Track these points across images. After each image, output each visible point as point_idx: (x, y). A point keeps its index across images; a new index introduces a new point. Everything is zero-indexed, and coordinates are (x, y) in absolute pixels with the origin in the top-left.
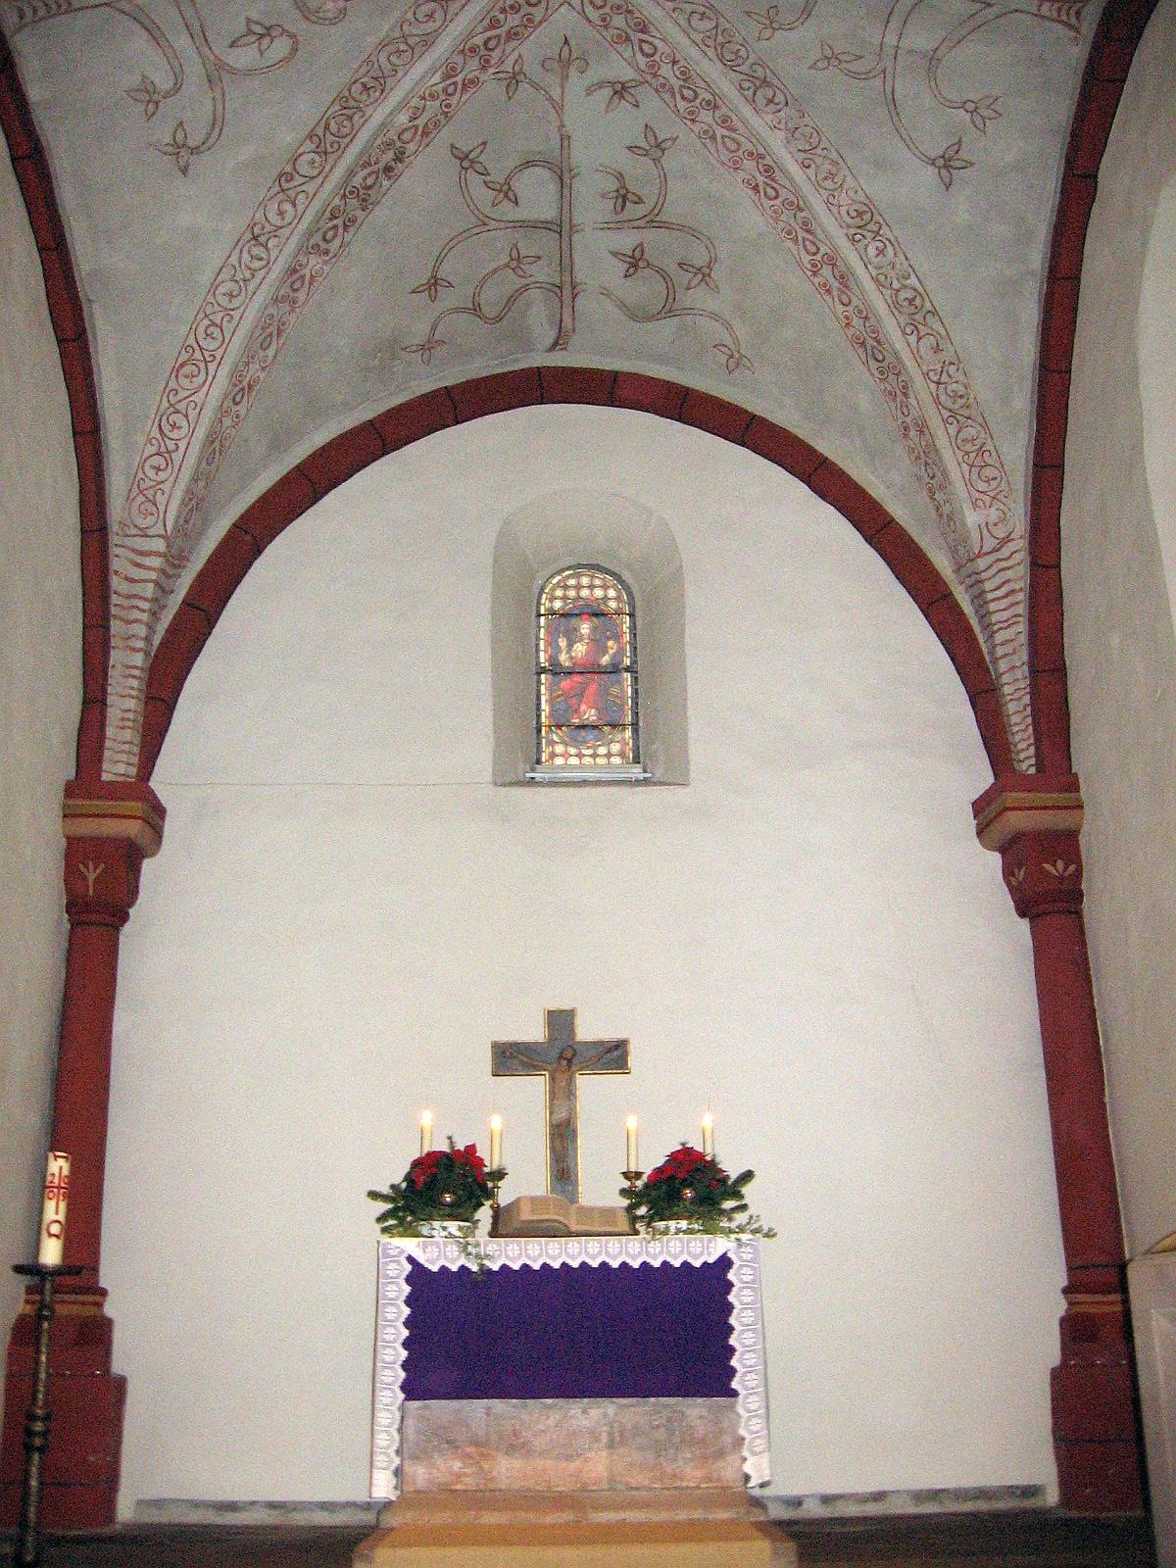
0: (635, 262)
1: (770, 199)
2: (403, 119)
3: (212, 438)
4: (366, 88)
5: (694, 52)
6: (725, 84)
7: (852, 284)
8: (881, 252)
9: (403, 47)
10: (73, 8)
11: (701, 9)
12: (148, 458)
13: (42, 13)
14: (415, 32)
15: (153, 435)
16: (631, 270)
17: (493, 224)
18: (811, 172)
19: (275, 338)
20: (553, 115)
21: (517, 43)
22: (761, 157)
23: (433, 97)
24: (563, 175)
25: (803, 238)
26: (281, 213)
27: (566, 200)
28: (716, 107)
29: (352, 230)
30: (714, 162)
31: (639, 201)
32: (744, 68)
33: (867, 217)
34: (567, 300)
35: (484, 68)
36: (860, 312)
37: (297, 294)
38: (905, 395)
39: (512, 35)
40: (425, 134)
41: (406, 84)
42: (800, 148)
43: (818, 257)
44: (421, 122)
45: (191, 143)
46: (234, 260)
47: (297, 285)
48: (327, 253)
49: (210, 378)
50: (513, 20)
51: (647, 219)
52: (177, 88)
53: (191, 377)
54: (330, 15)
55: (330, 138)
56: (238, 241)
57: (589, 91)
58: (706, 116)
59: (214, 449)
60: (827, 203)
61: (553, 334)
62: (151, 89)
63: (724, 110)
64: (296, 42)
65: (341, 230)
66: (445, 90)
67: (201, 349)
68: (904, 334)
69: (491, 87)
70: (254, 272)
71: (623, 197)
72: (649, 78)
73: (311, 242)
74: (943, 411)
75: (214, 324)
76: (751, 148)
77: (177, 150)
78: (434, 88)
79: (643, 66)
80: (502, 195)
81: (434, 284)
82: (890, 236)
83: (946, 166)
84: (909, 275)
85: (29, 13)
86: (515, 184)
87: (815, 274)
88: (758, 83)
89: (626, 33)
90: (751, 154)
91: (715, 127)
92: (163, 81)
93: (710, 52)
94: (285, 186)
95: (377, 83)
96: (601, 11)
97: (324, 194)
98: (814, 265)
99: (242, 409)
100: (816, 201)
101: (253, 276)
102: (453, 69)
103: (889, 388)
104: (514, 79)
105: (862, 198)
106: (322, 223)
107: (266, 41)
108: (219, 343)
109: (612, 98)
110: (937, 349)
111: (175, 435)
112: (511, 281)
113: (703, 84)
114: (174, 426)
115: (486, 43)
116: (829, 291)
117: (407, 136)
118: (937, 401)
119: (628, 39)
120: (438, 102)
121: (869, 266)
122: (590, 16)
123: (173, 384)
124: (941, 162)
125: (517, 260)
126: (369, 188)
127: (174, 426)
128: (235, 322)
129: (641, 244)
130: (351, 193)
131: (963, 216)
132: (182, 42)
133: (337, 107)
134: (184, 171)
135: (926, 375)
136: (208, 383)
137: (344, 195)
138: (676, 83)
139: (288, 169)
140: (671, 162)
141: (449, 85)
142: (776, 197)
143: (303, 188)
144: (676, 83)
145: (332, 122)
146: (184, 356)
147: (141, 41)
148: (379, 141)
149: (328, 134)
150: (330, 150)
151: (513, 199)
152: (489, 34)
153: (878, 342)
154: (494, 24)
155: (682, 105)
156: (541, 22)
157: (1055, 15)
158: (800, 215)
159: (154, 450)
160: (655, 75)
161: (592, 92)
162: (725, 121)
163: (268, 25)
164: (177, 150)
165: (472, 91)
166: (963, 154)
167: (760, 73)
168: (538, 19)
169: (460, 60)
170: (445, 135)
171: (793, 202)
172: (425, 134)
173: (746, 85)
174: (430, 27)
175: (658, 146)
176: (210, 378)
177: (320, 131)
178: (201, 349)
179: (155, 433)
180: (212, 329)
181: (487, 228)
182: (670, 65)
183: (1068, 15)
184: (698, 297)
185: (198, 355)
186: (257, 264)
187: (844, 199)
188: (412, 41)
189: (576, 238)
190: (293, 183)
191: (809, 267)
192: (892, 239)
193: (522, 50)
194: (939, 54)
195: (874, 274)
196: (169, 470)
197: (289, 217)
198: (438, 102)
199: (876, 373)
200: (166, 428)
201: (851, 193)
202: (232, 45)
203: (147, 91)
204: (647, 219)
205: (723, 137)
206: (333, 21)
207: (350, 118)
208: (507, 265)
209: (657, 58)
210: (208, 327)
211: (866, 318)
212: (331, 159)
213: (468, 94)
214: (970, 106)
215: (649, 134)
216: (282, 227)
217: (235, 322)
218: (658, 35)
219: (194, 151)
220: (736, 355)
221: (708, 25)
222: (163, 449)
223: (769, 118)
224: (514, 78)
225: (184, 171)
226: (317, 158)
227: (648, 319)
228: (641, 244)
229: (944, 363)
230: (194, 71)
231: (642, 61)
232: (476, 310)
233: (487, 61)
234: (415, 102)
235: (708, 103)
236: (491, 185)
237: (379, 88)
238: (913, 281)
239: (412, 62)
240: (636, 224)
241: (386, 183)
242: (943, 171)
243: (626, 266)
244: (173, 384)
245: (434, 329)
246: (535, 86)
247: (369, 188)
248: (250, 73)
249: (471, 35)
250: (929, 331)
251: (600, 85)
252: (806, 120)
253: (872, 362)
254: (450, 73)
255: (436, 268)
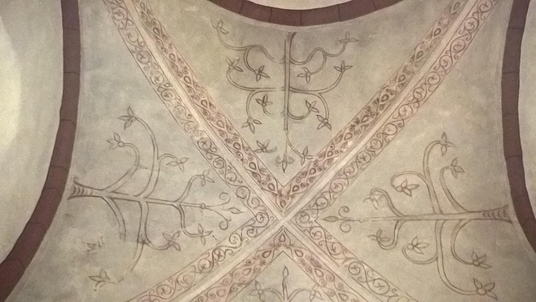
0: (260, 73)
1: (205, 100)
2: (350, 143)
3: (455, 15)
4: (364, 159)
5: (234, 164)
6: (223, 151)
7: (169, 64)
8: (157, 79)
9: (348, 174)
10: (482, 213)
11: (231, 183)
12: (488, 11)
13: (496, 213)
14: (343, 180)
15: (483, 21)
16: (261, 69)
17: (316, 93)
18: (188, 113)
19: (416, 54)
20: (290, 139)
21: (303, 171)
22: (208, 119)
23: (337, 152)
24: (287, 113)
25: (191, 83)
26: (405, 111)
27: (286, 102)
28: (226, 140)
29: (375, 98)
30: (227, 116)
31: (257, 100)
32: (215, 157)
33: (164, 94)
34: (288, 56)
35: (317, 161)
36: (165, 51)
37: (402, 74)
38: (142, 13)
39: (305, 174)
40: (341, 136)
41: (348, 158)
42: (192, 123)
43: (184, 75)
44: (343, 141)
45: (440, 146)
46: (429, 93)
47: (402, 78)
48: (387, 90)
49: (450, 44)
50: (304, 180)
51: (255, 92)
52: (443, 171)
53: (458, 45)
54: (377, 193)
55: (381, 139)
56: (425, 101)
57: (276, 149)
58: (231, 136)
59: (454, 9)
60: (180, 100)
61: (294, 40)
62: (454, 172)
63: (223, 139)
64: (391, 183)
65: (380, 100)
66: (332, 154)
67: (451, 57)
68: (145, 42)
69: (314, 153)
70: (421, 87)
71: (264, 102)
72: (252, 153)
73: (394, 96)
74: (124, 6)
75: (443, 67)
76: (212, 123)
77: (446, 144)
78: (337, 155)
79: (255, 158)
80: (312, 106)
81: (342, 69)
82: (154, 86)
83: (131, 117)
84: (144, 69)
85: (501, 213)
86: (307, 111)
87: (186, 68)
88: (209, 151)
89: (261, 173)
90: (212, 120)
91: (227, 132)
92: (448, 173)
93: (228, 164)
94: (402, 122)
95: (359, 160)
96: (270, 182)
97: (386, 117)
98: (186, 72)
99: (437, 26)
100: (185, 101)
101: (422, 85)
102: (329, 162)
103: (150, 16)
104: (305, 154)
105: (165, 102)
106: (388, 104)
107: (404, 185)
108: (443, 58)
109: (267, 145)
110: (129, 35)
111: (473, 20)
112: (311, 66)
113: (231, 150)
114: (472, 24)
115: (315, 172)
116: (179, 60)
117: (349, 136)
118: (127, 11)
119: (260, 170)
120: (336, 149)
121: (162, 72)
122: (275, 181)
123: (468, 42)
124: (133, 119)
125: (307, 75)
126: (365, 116)
127: (472, 24)
128: (433, 67)
129: (257, 81)
130: (374, 115)
131: (122, 95)
132: (439, 190)
133: (377, 152)
134: (444, 134)
135: (133, 23)
136: (451, 42)
137: (377, 114)
138: (242, 151)
139: (399, 129)
140: (245, 117)
141: (330, 156)
142: (202, 101)
143: (394, 120)
144: (242, 151)
145: (379, 146)
146: (459, 55)
147: (455, 193)
148: (360, 135)
149: (381, 141)
150: (381, 135)
151: (308, 104)
152: (314, 175)
153: (156, 37)
154: (311, 179)
155: (240, 142)
156: (293, 179)
157: (85, 189)
158: (192, 94)
159: (485, 14)
160: (250, 154)
161: (275, 148)
162: (222, 133)
163: (403, 192)
164: (446, 144)
165: (321, 152)
166: (123, 122)
167: (209, 156)
168: (295, 180)
169: (326, 166)
170: (334, 134)
171: (195, 99)
172: (341, 136)
173: (214, 150)
174: (337, 181)
175: (250, 124)
176: (450, 44)
177: (385, 143)
178: (451, 57)
179: (481, 22)
180: (444, 65)
181: (319, 92)
182: (244, 158)
183: (79, 190)
184: (233, 55)
185: (453, 54)
186: (419, 90)
187: (174, 102)
188: (344, 176)
189: (283, 85)
190: (399, 122)
191: (188, 71)
192: (152, 84)
193: (301, 167)
194: (135, 167)
195: (160, 69)
196: (480, 4)
197: (402, 109)
198: (336, 149)
199: (157, 22)
200: (476, 24)
201: (171, 104)
202: (418, 186)
203: (455, 170)
204: (255, 92)
205: (224, 127)
206: (377, 190)
207: (371, 147)
208: (311, 74)
209: (249, 162)
210: (446, 66)
211: (162, 48)
212: (381, 131)
213: (323, 151)
214: (121, 144)
215: (253, 129)
216: (406, 105)
217: (433, 67)
218: (248, 171)
219: (438, 142)
220: (219, 29)
221: (229, 176)
222: (480, 14)
223: (205, 136)
224: (305, 156)
225: (444, 134)
226: (387, 132)
227: (255, 46)
228: (257, 81)
229: (125, 29)
230: (435, 176)
231: (255, 161)
232: (326, 55)
233: (315, 164)
234: (344, 150)
235: (229, 142)
236: (317, 111)
237: (359, 158)
238: (142, 66)
239: (345, 166)
240: (259, 90)
241: (359, 117)
242: (132, 115)
243: (263, 71)
244: (468, 42)
245: (344, 49)
246: (296, 152)
247: (365, 116)
248: (411, 173)
249: (321, 176)
250: (133, 44)
251: (271, 151)
252: (190, 135)
253: (159, 28)
254: (330, 161)
255: (341, 76)
